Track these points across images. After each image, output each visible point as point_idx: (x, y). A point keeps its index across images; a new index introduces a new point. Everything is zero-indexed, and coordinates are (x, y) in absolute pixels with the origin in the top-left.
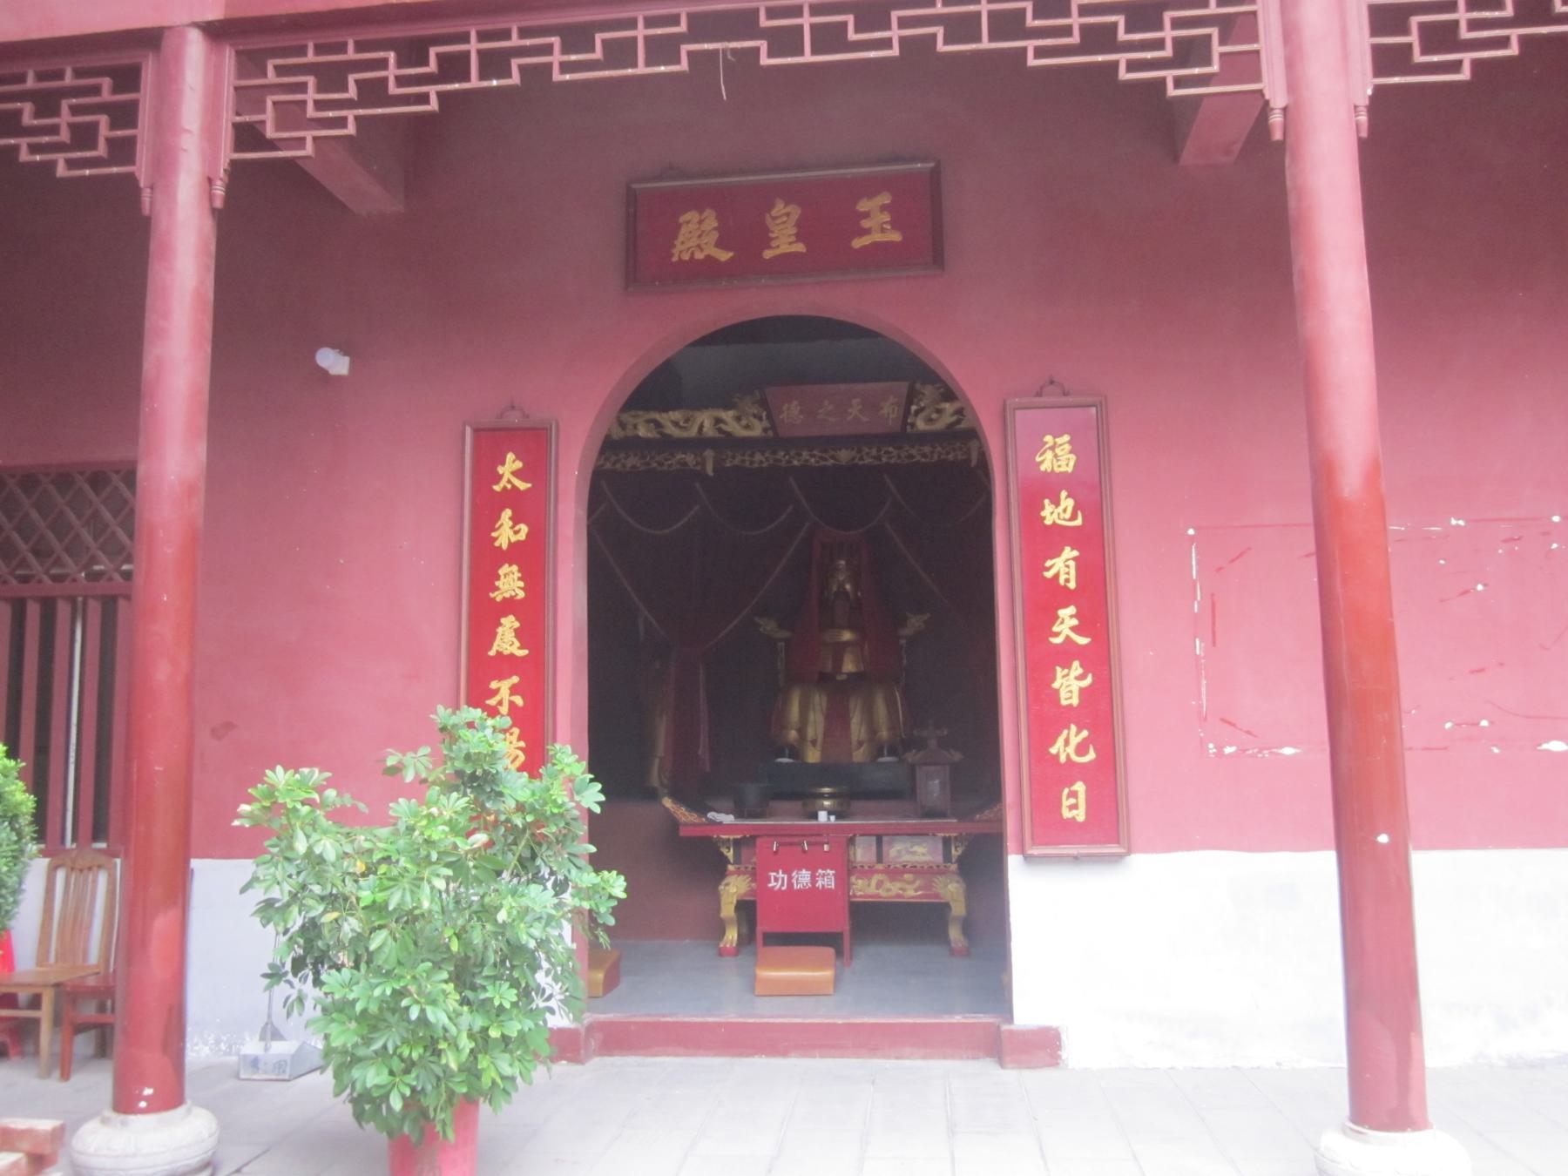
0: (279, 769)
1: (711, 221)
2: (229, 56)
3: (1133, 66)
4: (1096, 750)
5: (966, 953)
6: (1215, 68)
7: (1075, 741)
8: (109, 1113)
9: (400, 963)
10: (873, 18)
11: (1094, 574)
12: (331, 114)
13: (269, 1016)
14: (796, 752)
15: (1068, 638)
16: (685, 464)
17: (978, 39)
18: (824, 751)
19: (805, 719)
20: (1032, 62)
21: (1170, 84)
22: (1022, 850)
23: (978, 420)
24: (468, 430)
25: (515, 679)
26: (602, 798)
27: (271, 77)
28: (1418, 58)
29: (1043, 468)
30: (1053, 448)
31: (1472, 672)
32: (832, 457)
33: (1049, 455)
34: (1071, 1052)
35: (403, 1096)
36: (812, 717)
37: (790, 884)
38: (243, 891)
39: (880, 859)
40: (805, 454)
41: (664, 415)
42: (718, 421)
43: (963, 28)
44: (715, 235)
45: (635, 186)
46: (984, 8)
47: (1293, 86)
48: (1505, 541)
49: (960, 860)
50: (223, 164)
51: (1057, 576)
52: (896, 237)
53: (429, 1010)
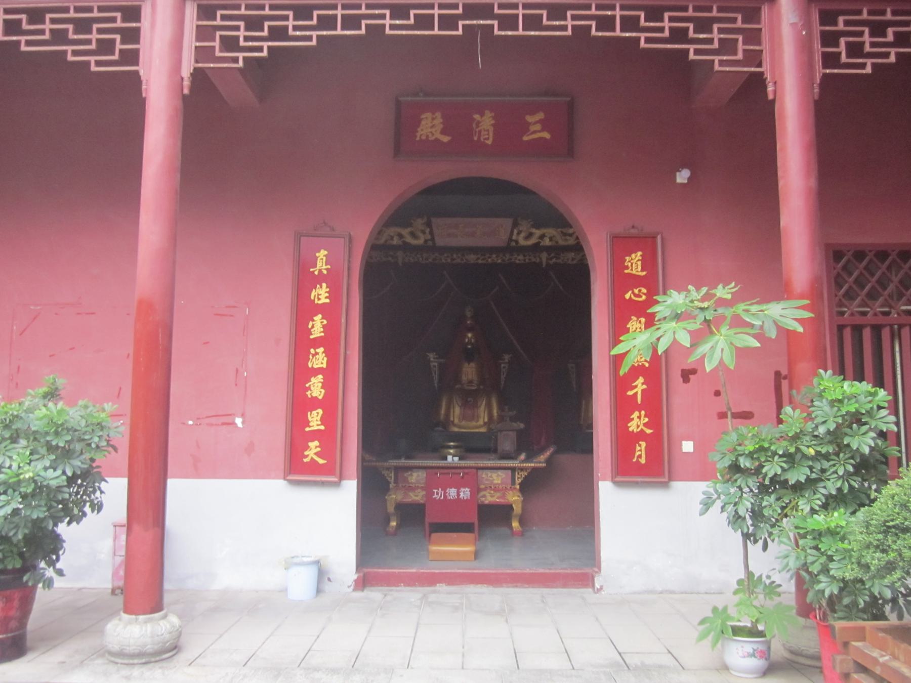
1: (439, 120)
3: (75, 53)
5: (522, 534)
17: (335, 29)
28: (218, 54)
37: (445, 496)
43: (606, 23)
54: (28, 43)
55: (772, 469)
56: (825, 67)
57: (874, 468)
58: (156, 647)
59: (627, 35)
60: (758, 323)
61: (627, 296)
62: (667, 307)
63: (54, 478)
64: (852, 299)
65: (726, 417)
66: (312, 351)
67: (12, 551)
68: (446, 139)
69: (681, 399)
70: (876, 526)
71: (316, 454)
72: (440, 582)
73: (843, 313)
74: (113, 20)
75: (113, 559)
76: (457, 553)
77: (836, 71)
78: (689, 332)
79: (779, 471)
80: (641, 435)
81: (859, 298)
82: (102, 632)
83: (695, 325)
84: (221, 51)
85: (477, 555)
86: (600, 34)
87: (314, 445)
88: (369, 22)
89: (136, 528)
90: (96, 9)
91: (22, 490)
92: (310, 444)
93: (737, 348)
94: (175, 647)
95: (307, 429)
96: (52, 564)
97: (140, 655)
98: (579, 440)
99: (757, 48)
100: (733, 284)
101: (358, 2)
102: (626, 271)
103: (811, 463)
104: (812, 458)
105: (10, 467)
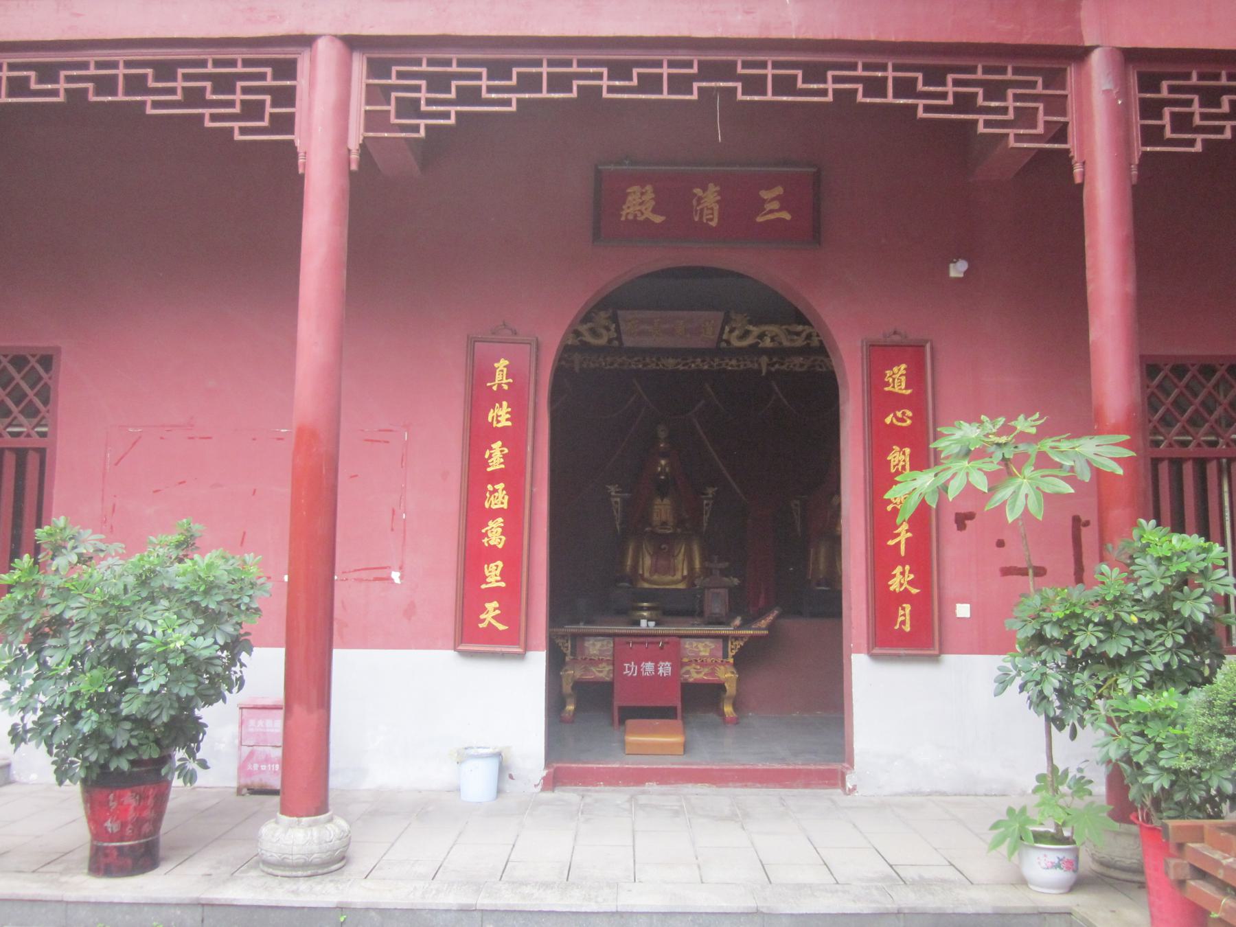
1: (650, 195)
3: (214, 118)
5: (736, 722)
17: (115, 93)
44: (652, 204)
54: (156, 105)
55: (1086, 640)
56: (1144, 144)
57: (1207, 641)
58: (324, 856)
59: (902, 101)
60: (1068, 463)
61: (888, 420)
62: (958, 441)
63: (204, 646)
64: (1169, 425)
65: (1027, 574)
66: (490, 487)
67: (147, 738)
68: (658, 219)
69: (955, 550)
70: (1221, 707)
71: (495, 618)
72: (649, 780)
73: (1157, 444)
74: (262, 77)
75: (240, 749)
76: (662, 745)
77: (1158, 149)
78: (986, 473)
79: (1095, 643)
80: (905, 596)
81: (1179, 425)
82: (255, 839)
83: (993, 466)
84: (398, 116)
85: (686, 748)
86: (868, 100)
87: (492, 607)
88: (582, 82)
89: (298, 709)
90: (239, 63)
91: (171, 662)
92: (488, 605)
93: (1045, 494)
94: (343, 858)
95: (484, 586)
96: (192, 754)
97: (305, 865)
98: (829, 605)
99: (1062, 119)
100: (1037, 415)
102: (887, 389)
103: (1133, 633)
104: (1133, 627)
105: (153, 634)
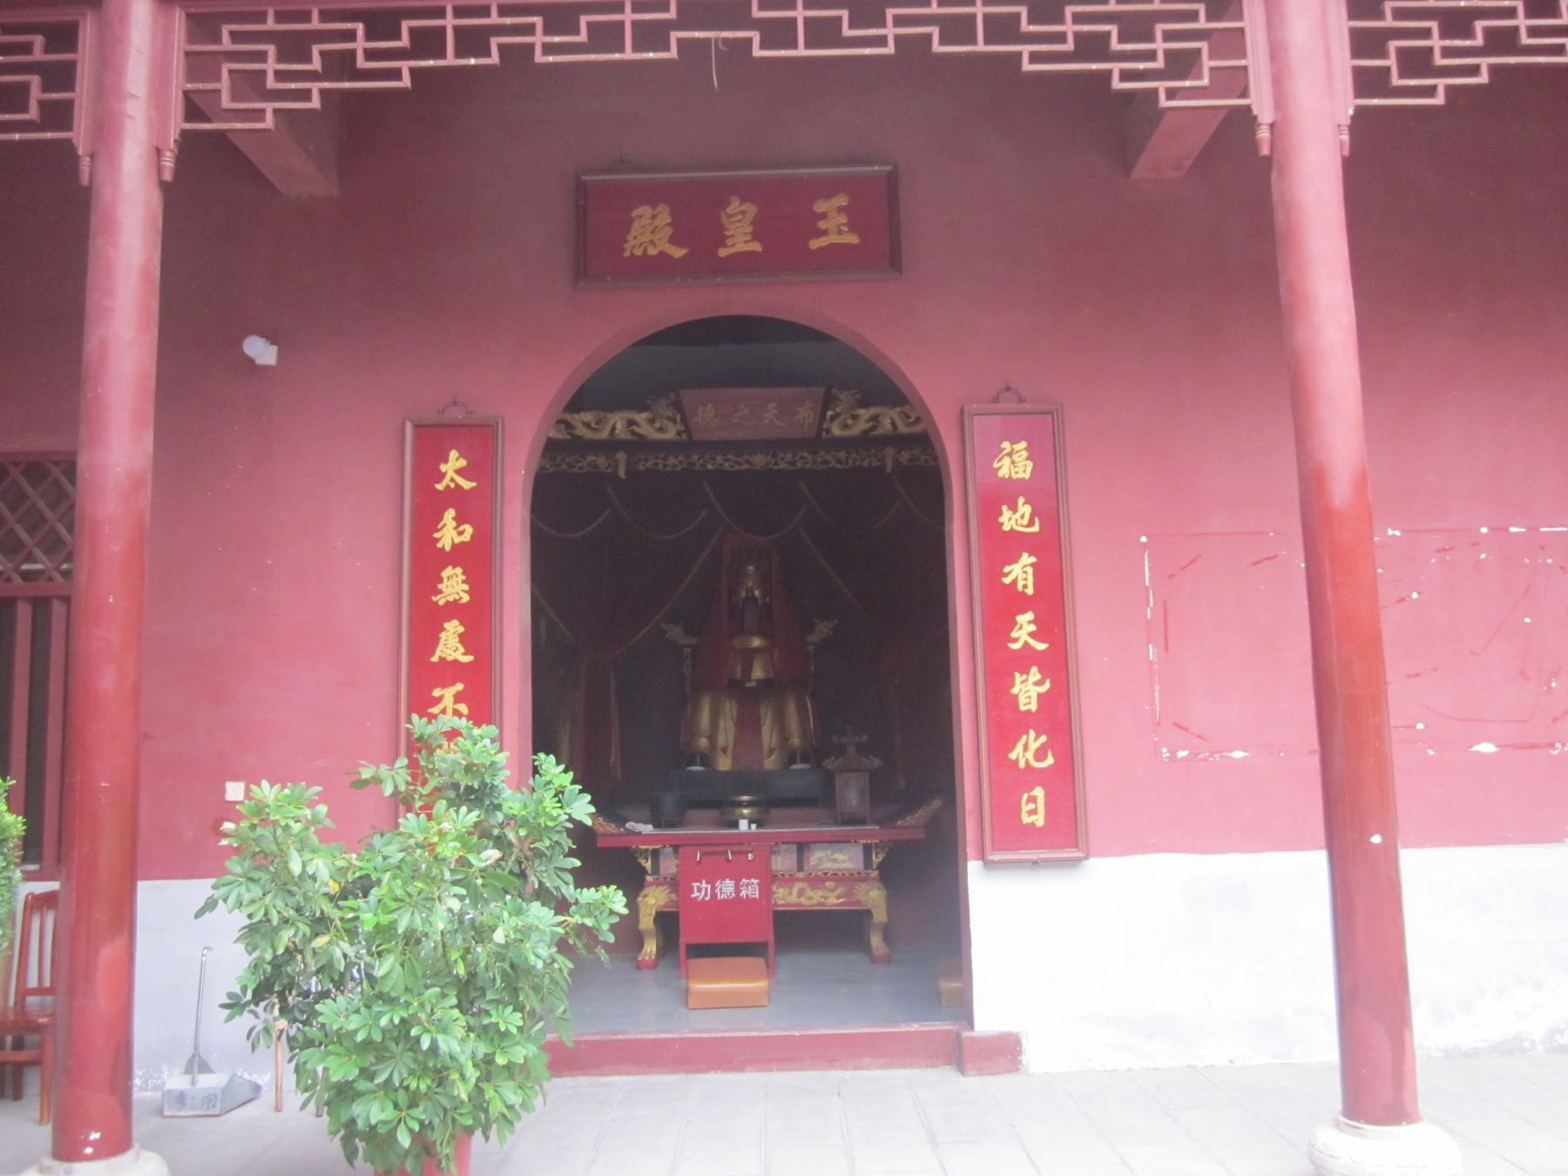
0: (265, 783)
1: (664, 216)
2: (179, 18)
3: (1126, 76)
4: (1054, 756)
5: (887, 960)
6: (1205, 81)
7: (1033, 746)
8: (49, 1162)
9: (407, 989)
10: (868, 14)
11: (1051, 579)
12: (293, 86)
13: (196, 1047)
14: (706, 760)
15: (1026, 643)
16: (597, 466)
18: (735, 758)
19: (716, 727)
20: (1027, 66)
21: (1162, 96)
22: (982, 856)
23: (933, 422)
24: (409, 427)
25: (459, 687)
26: (593, 809)
27: (227, 44)
28: (1396, 81)
29: (1001, 474)
30: (1010, 454)
31: (1408, 677)
32: (748, 462)
33: (1007, 461)
34: (1032, 1057)
35: (411, 1131)
36: (722, 725)
37: (714, 895)
38: (198, 915)
39: (800, 868)
40: (719, 458)
41: (576, 416)
42: (631, 423)
43: (958, 29)
44: (669, 231)
45: (585, 178)
46: (979, 10)
47: (1280, 102)
48: (1438, 551)
49: (880, 866)
50: (173, 136)
51: (1015, 582)
52: (853, 239)
53: (440, 1038)
84: (1402, 75)
101: (439, 3)
